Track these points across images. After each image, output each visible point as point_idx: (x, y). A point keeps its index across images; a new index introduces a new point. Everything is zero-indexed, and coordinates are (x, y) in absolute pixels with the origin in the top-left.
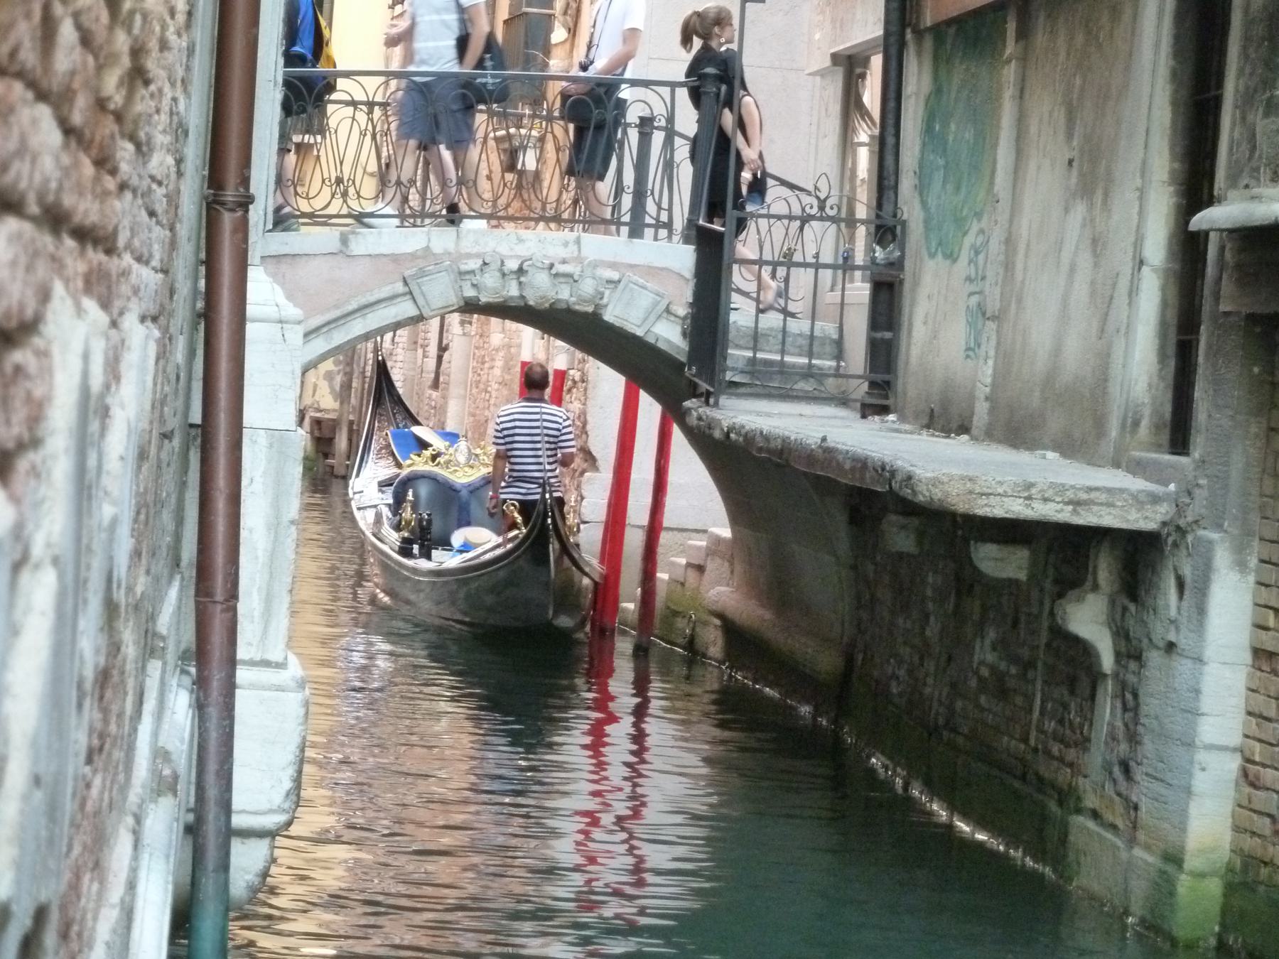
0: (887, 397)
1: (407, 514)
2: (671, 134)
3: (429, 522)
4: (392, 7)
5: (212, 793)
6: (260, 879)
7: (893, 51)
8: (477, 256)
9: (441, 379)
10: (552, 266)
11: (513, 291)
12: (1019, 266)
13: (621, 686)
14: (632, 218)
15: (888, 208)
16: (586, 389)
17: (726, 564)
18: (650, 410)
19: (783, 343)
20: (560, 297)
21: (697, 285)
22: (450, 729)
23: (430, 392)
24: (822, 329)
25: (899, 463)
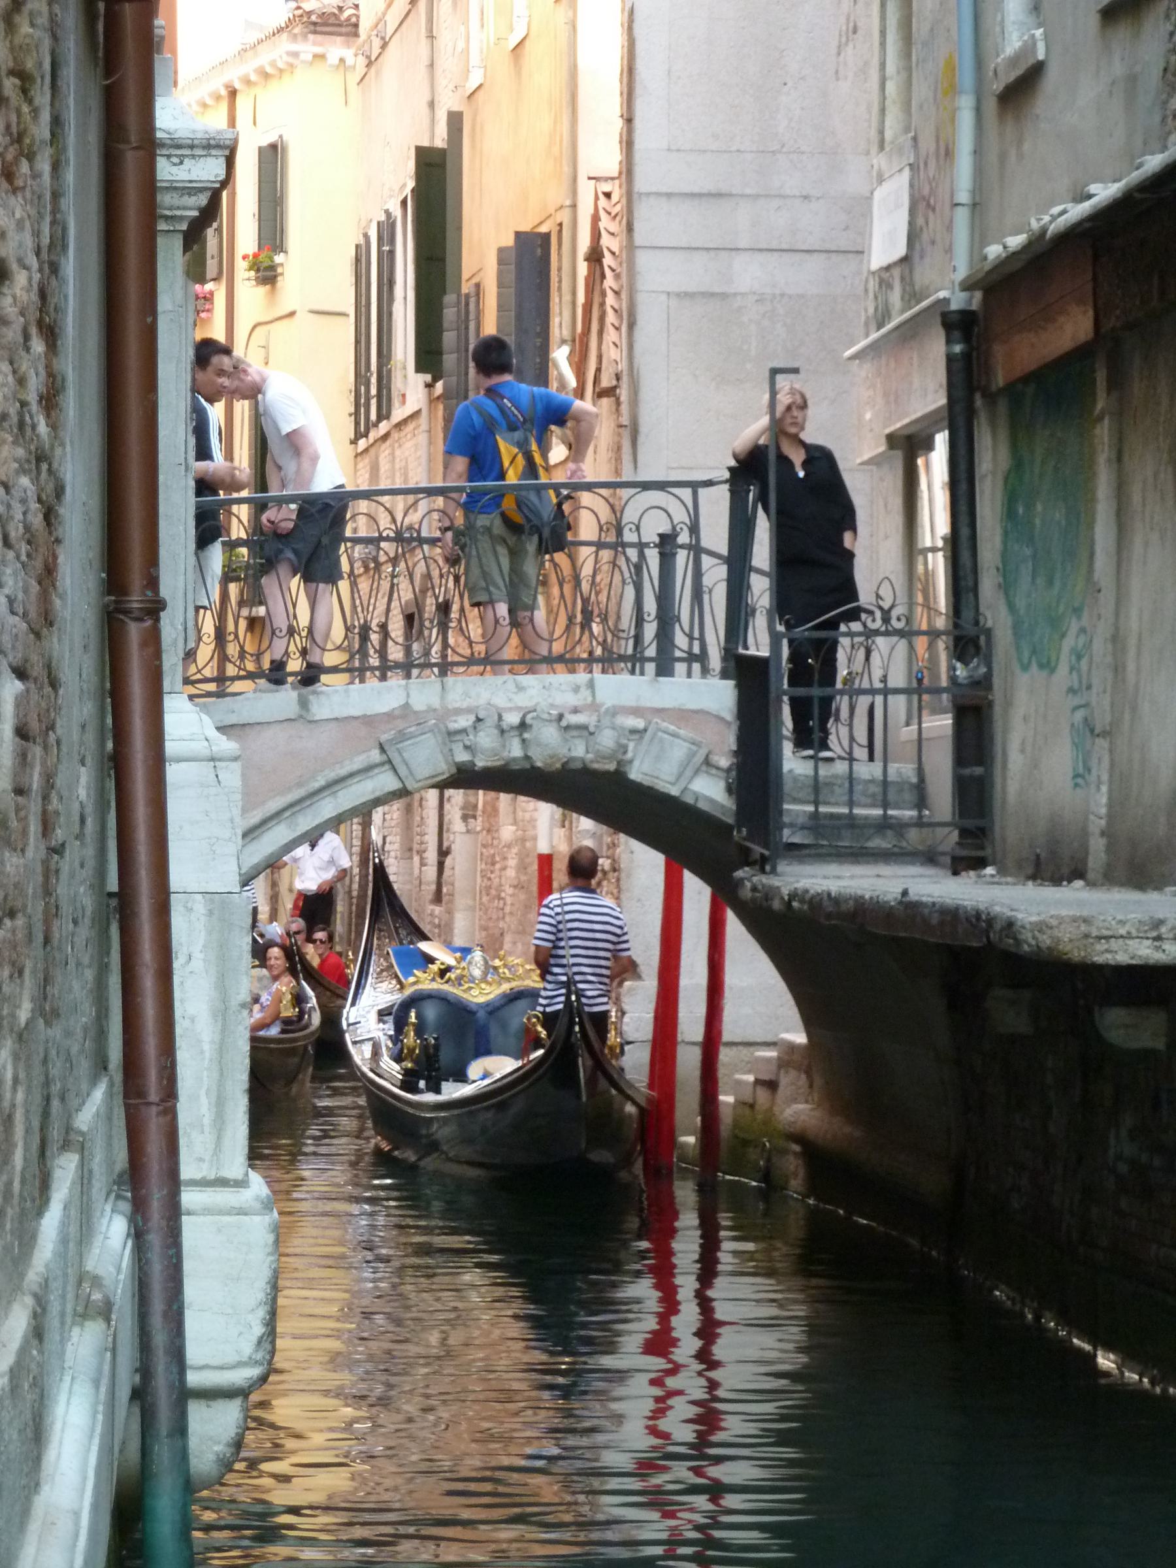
0: (982, 848)
1: (410, 1039)
2: (697, 550)
3: (437, 1047)
4: (354, 442)
5: (160, 1339)
6: (233, 1450)
7: (961, 421)
8: (469, 710)
9: (445, 890)
10: (561, 717)
11: (515, 750)
12: (1131, 667)
13: (686, 1248)
14: (659, 650)
15: (967, 614)
16: (618, 880)
17: (803, 1076)
18: (697, 894)
19: (851, 791)
20: (574, 754)
21: (741, 729)
22: (483, 1317)
23: (432, 907)
24: (899, 773)
25: (997, 909)
